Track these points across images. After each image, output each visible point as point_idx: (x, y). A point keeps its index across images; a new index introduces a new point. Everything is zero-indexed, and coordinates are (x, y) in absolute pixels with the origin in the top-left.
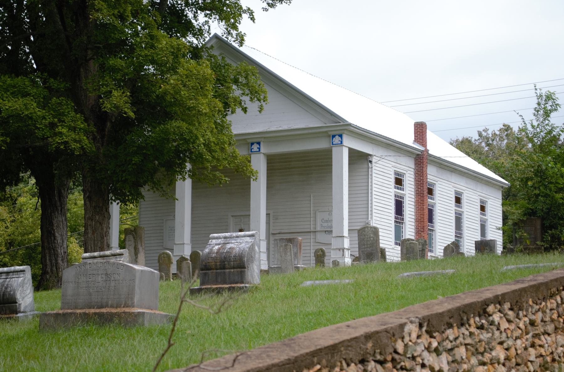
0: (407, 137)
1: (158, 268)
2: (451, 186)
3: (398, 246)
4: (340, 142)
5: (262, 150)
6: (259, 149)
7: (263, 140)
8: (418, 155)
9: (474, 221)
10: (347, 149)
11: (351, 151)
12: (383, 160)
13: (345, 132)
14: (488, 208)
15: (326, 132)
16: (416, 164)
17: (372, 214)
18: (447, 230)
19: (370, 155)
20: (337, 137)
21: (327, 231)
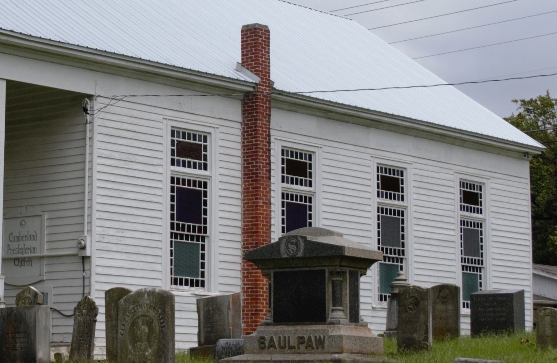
0: (223, 59)
1: (307, 255)
12: (121, 103)
14: (488, 199)
16: (244, 112)
19: (90, 97)
21: (17, 259)
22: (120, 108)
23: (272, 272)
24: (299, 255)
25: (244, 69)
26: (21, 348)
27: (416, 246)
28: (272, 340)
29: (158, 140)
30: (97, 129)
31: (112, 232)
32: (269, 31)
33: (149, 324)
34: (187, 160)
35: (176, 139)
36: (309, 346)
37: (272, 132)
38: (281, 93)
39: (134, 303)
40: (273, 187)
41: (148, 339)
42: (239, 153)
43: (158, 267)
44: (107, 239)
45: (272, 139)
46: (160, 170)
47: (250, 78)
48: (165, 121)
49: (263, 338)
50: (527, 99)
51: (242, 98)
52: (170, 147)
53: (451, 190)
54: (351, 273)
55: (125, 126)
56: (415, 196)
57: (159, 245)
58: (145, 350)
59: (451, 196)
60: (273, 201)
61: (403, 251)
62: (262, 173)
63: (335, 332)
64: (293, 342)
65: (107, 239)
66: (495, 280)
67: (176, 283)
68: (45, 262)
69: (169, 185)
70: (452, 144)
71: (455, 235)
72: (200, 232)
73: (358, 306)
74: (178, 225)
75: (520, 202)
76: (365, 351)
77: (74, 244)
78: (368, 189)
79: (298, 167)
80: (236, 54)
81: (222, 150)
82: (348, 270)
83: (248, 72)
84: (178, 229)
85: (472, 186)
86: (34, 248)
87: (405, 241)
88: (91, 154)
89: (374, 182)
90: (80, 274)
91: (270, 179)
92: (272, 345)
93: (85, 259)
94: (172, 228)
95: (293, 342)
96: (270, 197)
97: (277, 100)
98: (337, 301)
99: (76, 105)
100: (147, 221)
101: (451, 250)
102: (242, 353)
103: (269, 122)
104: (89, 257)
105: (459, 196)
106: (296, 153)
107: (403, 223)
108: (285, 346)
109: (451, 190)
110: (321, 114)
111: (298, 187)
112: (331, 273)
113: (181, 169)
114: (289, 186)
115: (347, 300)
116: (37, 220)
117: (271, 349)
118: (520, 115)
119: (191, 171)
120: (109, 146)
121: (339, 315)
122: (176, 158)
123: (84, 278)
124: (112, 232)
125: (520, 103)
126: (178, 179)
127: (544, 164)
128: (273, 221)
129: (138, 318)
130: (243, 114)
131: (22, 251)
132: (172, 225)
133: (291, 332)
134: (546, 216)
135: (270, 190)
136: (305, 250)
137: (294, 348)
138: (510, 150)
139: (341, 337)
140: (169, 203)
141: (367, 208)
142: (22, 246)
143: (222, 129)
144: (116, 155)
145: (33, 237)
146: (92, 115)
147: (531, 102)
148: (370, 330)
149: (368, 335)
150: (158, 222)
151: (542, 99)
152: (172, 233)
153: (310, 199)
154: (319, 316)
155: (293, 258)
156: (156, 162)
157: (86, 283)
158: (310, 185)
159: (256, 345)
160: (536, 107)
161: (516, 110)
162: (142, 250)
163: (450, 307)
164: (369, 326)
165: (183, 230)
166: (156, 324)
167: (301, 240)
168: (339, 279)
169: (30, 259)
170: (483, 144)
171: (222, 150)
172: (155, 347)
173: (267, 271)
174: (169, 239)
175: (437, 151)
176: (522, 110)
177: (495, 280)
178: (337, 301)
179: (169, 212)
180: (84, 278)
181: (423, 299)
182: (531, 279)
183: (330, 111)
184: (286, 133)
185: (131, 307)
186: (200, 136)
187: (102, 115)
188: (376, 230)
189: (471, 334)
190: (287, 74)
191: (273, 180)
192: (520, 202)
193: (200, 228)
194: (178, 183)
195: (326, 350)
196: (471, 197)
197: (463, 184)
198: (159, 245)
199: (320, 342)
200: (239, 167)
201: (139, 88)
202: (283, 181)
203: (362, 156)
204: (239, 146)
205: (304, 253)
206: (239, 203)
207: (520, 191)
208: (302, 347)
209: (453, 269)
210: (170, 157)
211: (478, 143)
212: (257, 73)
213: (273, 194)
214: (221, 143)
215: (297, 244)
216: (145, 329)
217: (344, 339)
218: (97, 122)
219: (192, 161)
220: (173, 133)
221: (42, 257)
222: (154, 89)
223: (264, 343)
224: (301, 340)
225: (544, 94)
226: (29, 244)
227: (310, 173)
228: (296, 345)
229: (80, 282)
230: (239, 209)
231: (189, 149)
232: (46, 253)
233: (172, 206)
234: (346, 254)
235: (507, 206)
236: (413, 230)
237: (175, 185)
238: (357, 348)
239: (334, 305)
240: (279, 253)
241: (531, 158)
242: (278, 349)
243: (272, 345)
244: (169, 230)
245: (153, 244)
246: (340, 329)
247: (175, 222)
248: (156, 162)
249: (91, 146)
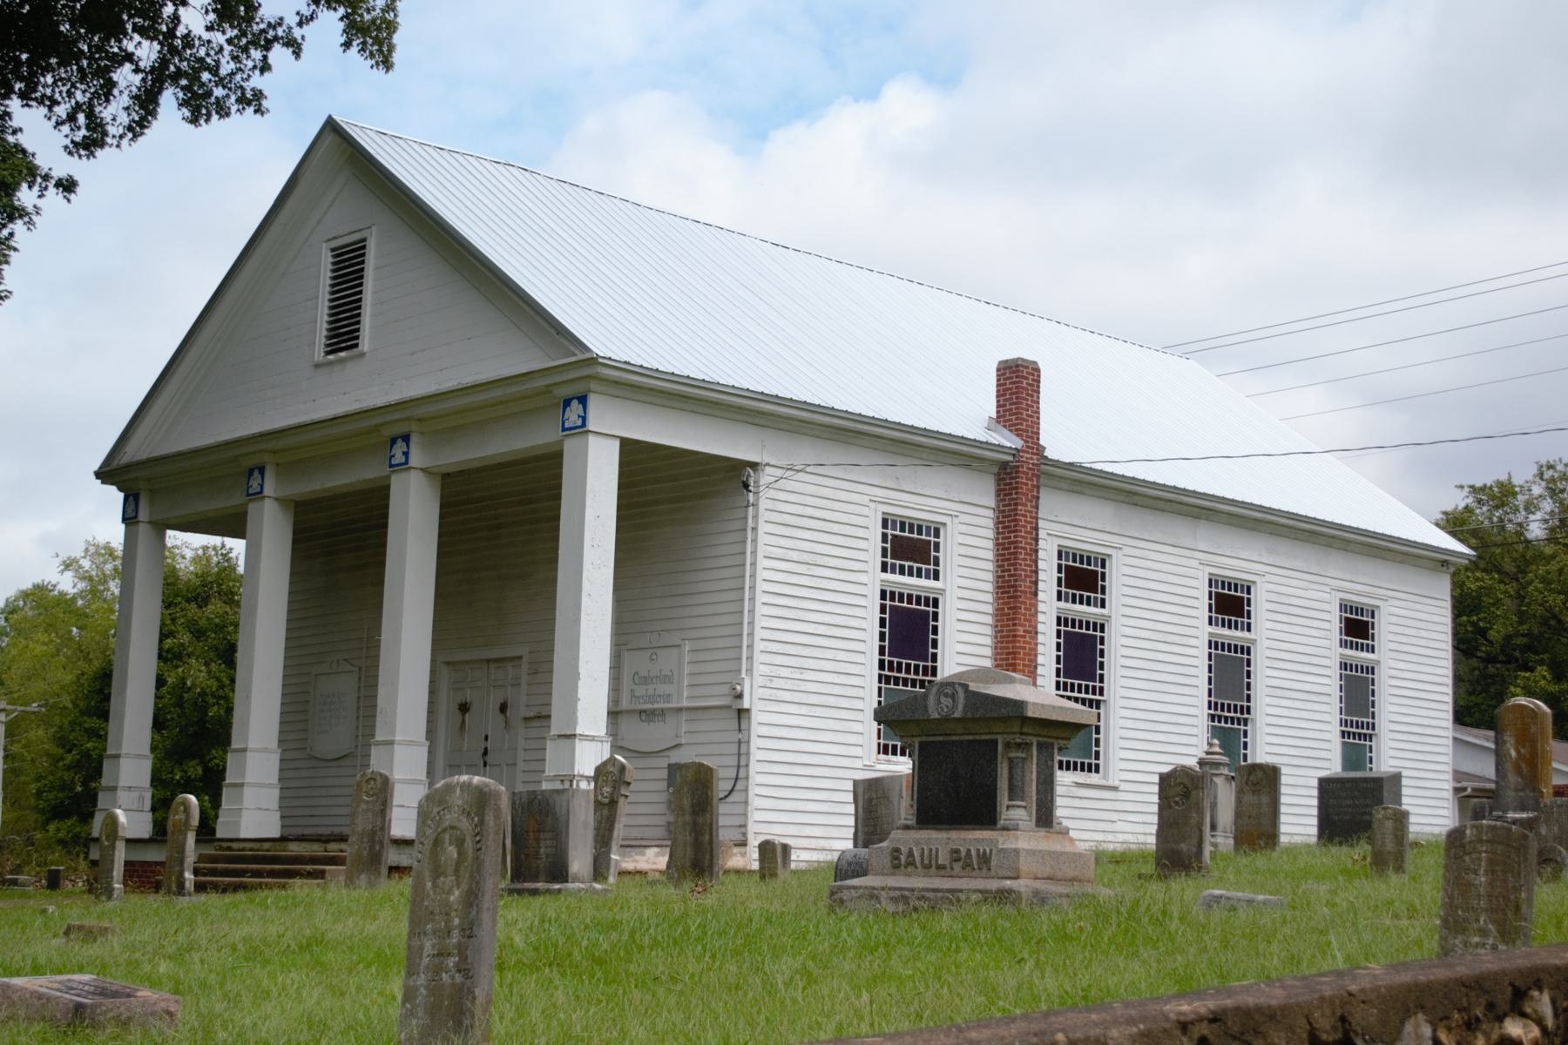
0: (969, 412)
1: (969, 715)
2: (1195, 563)
3: (899, 758)
4: (579, 423)
5: (416, 460)
6: (406, 454)
7: (414, 427)
8: (1005, 464)
9: (1422, 651)
10: (615, 446)
11: (632, 452)
12: (801, 476)
13: (593, 386)
14: (1384, 630)
15: (548, 390)
16: (999, 492)
17: (750, 658)
18: (1167, 698)
19: (754, 466)
20: (575, 403)
21: (644, 711)
22: (801, 483)
23: (916, 741)
24: (957, 714)
25: (1000, 427)
26: (547, 856)
27: (1268, 700)
28: (911, 854)
29: (861, 533)
30: (764, 515)
31: (784, 672)
32: (1038, 370)
33: (459, 843)
34: (907, 564)
35: (889, 532)
36: (968, 865)
37: (1041, 524)
38: (1057, 464)
39: (440, 803)
40: (1041, 607)
41: (457, 870)
42: (990, 555)
43: (857, 727)
44: (777, 683)
45: (1042, 534)
46: (863, 578)
47: (1009, 440)
48: (872, 505)
49: (897, 850)
50: (1479, 484)
51: (996, 470)
52: (880, 544)
53: (1326, 616)
54: (1040, 746)
55: (809, 511)
56: (1269, 625)
57: (860, 693)
58: (450, 892)
59: (1327, 625)
60: (1040, 628)
61: (1248, 708)
62: (1024, 585)
63: (1005, 841)
64: (943, 858)
65: (777, 683)
66: (1393, 753)
67: (886, 752)
68: (684, 716)
69: (878, 601)
70: (1329, 546)
71: (1331, 684)
72: (926, 673)
73: (1052, 801)
74: (891, 663)
75: (1435, 635)
76: (1059, 875)
77: (726, 689)
78: (1193, 612)
79: (1083, 578)
80: (986, 402)
81: (963, 550)
82: (1034, 740)
83: (1006, 432)
84: (891, 669)
85: (1359, 610)
86: (669, 695)
87: (1252, 692)
88: (754, 553)
89: (1204, 602)
90: (735, 736)
91: (1036, 594)
92: (911, 863)
93: (742, 713)
94: (881, 667)
95: (943, 858)
96: (1037, 622)
97: (1051, 476)
98: (1015, 792)
99: (734, 477)
100: (842, 656)
101: (1324, 708)
102: (865, 873)
103: (1037, 507)
104: (748, 710)
105: (1338, 625)
106: (1082, 557)
107: (1249, 665)
108: (931, 865)
109: (1326, 616)
110: (1121, 498)
111: (1084, 608)
112: (1007, 745)
113: (897, 578)
114: (1069, 605)
115: (1032, 790)
116: (675, 650)
117: (910, 869)
118: (1466, 507)
119: (914, 581)
120: (782, 542)
121: (1018, 814)
122: (889, 560)
123: (740, 742)
124: (784, 672)
125: (1467, 489)
126: (893, 594)
127: (1501, 582)
128: (1040, 659)
129: (444, 830)
130: (998, 495)
131: (652, 698)
132: (881, 663)
133: (941, 840)
134: (1501, 658)
135: (1037, 612)
136: (965, 706)
137: (943, 867)
138: (1420, 557)
139: (1017, 852)
140: (877, 629)
141: (1193, 642)
142: (651, 692)
143: (963, 518)
144: (794, 555)
145: (667, 679)
146: (756, 493)
147: (1483, 489)
148: (1072, 840)
149: (1069, 849)
150: (860, 658)
151: (1500, 484)
152: (880, 676)
153: (1102, 626)
154: (983, 814)
155: (946, 720)
156: (857, 566)
157: (743, 750)
158: (1103, 606)
159: (887, 861)
160: (1493, 498)
161: (1458, 500)
162: (832, 701)
163: (1265, 799)
164: (1072, 834)
165: (899, 671)
166: (469, 844)
167: (960, 691)
168: (1020, 755)
169: (663, 712)
170: (1377, 547)
171: (963, 550)
172: (464, 886)
173: (909, 740)
174: (876, 685)
175: (1301, 557)
176: (1470, 500)
177: (1393, 753)
178: (1015, 792)
179: (877, 643)
180: (740, 742)
181: (1196, 788)
182: (1450, 750)
183: (1136, 494)
184: (1062, 527)
185: (436, 810)
186: (928, 528)
187: (772, 493)
188: (1206, 674)
189: (1320, 836)
190: (1062, 437)
191: (1041, 596)
192: (1435, 635)
193: (926, 668)
194: (892, 599)
195: (993, 873)
196: (1357, 628)
197: (1344, 607)
198: (860, 693)
199: (985, 859)
200: (990, 577)
201: (834, 454)
202: (1059, 599)
203: (1184, 561)
204: (990, 544)
205: (965, 711)
206: (989, 630)
207: (1436, 619)
208: (957, 867)
209: (1327, 736)
210: (879, 559)
211: (1369, 545)
212: (1019, 433)
213: (1041, 617)
214: (962, 539)
215: (953, 697)
216: (452, 851)
217: (1022, 854)
218: (764, 504)
219: (915, 565)
220: (885, 524)
221: (680, 710)
222: (855, 455)
223: (897, 858)
224: (955, 855)
225: (1503, 478)
226: (663, 689)
227: (1103, 588)
228: (947, 863)
229: (734, 749)
230: (988, 641)
231: (910, 547)
232: (685, 703)
233: (882, 635)
234: (1030, 714)
235: (1414, 641)
236: (1265, 676)
237: (888, 602)
238: (1047, 871)
239: (1011, 799)
240: (926, 708)
241: (1452, 569)
242: (920, 869)
243: (911, 863)
244: (876, 671)
245: (850, 691)
246: (1017, 838)
247: (887, 658)
248: (857, 566)
249: (755, 541)
